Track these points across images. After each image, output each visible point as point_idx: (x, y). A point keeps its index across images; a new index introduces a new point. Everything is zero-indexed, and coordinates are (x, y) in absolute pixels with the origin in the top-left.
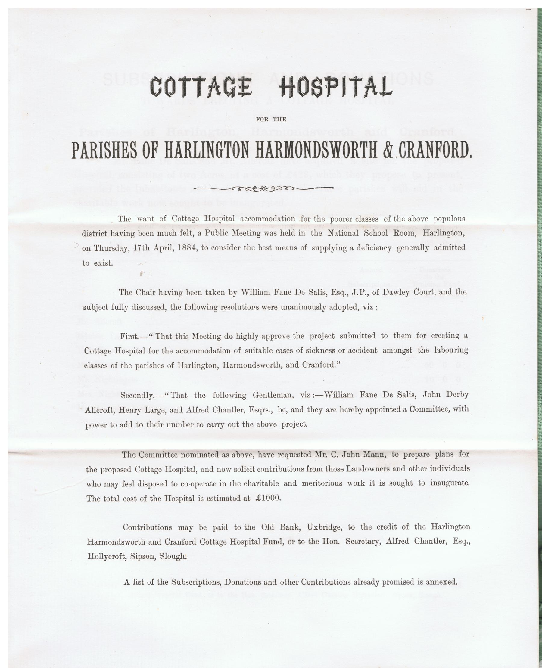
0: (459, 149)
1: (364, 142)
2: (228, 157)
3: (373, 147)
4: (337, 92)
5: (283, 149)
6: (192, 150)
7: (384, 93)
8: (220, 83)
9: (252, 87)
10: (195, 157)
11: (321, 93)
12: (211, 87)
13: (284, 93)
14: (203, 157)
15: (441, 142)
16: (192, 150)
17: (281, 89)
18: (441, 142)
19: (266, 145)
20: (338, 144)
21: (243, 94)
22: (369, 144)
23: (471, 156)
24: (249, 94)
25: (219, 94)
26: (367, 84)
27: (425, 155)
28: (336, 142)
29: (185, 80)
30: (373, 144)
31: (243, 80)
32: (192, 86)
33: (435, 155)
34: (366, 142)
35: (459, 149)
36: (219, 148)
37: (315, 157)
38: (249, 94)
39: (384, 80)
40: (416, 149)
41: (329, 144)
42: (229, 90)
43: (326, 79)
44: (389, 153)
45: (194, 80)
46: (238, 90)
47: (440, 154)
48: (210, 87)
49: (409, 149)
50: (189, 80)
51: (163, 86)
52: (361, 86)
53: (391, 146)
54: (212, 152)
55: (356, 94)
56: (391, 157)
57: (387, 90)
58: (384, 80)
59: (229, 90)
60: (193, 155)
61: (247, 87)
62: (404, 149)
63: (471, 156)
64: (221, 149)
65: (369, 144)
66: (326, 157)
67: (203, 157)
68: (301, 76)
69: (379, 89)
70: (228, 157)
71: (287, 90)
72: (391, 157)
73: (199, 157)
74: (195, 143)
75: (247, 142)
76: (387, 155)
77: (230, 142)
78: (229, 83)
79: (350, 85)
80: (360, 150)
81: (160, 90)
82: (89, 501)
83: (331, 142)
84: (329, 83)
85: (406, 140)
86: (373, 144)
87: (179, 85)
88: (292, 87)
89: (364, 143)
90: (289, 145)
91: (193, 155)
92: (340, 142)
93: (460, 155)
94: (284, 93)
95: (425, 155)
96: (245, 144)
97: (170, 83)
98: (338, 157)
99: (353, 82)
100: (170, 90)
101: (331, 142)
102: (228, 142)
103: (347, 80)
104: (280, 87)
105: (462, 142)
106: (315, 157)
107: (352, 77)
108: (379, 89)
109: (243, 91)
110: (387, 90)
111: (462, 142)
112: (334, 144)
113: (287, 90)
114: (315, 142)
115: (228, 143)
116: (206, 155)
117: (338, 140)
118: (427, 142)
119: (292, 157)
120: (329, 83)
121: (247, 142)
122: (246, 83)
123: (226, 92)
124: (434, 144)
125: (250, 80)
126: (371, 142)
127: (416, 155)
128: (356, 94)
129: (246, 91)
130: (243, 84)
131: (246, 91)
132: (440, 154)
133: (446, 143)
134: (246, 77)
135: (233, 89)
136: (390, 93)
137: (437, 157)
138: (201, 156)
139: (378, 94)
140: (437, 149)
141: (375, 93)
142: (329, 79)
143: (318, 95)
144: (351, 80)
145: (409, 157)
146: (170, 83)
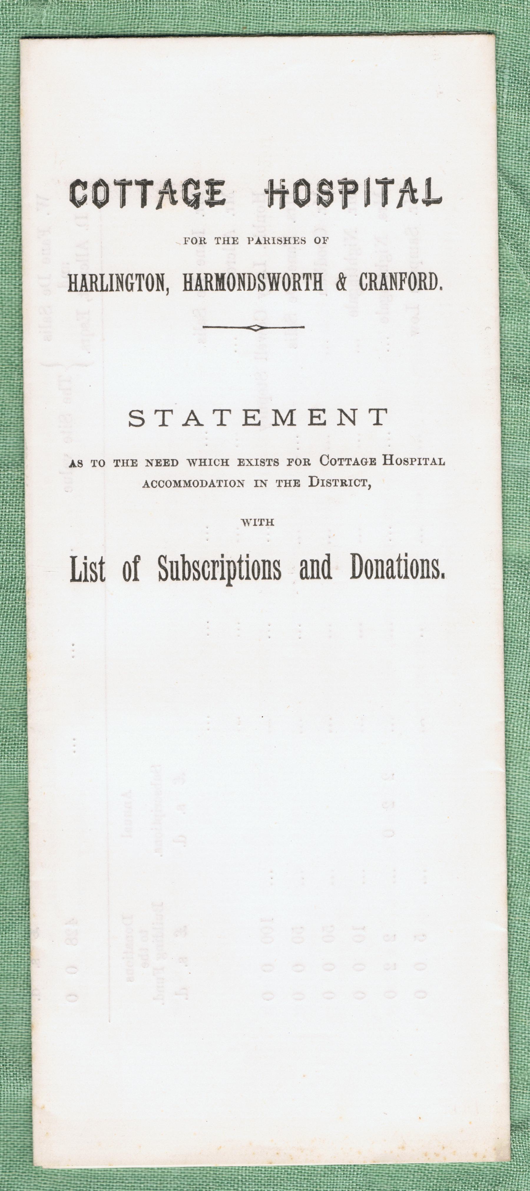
0: (428, 281)
1: (307, 274)
2: (140, 290)
3: (318, 279)
4: (357, 200)
5: (214, 282)
6: (99, 283)
7: (427, 203)
8: (177, 186)
9: (225, 192)
10: (102, 290)
11: (332, 200)
12: (162, 193)
13: (271, 203)
14: (112, 290)
15: (406, 274)
16: (99, 283)
17: (267, 196)
18: (406, 274)
19: (195, 277)
20: (276, 276)
21: (211, 204)
22: (313, 276)
23: (441, 288)
24: (222, 202)
25: (174, 202)
26: (402, 186)
27: (389, 287)
28: (274, 274)
29: (123, 184)
30: (318, 276)
31: (211, 183)
32: (134, 193)
33: (399, 287)
34: (310, 274)
35: (428, 281)
36: (130, 281)
37: (249, 289)
38: (222, 202)
39: (429, 181)
40: (379, 282)
41: (266, 276)
42: (191, 197)
43: (340, 183)
44: (343, 285)
45: (138, 183)
46: (204, 197)
47: (405, 286)
48: (160, 193)
49: (371, 280)
50: (130, 183)
51: (89, 192)
52: (394, 192)
53: (345, 278)
54: (122, 283)
55: (385, 203)
56: (344, 289)
57: (434, 196)
58: (429, 181)
59: (191, 197)
60: (99, 288)
61: (219, 192)
62: (366, 281)
63: (441, 288)
64: (132, 281)
65: (313, 276)
66: (262, 290)
67: (112, 290)
68: (296, 179)
69: (421, 195)
70: (140, 290)
71: (277, 198)
72: (344, 289)
73: (107, 290)
74: (102, 275)
75: (163, 275)
76: (340, 287)
77: (143, 275)
78: (191, 187)
79: (376, 190)
80: (303, 283)
81: (85, 198)
82: (440, 459)
83: (269, 274)
84: (346, 187)
85: (368, 271)
86: (318, 276)
87: (115, 192)
88: (283, 193)
89: (307, 276)
90: (220, 279)
91: (99, 288)
92: (279, 274)
93: (428, 287)
94: (271, 203)
95: (389, 287)
96: (161, 276)
97: (101, 190)
98: (277, 289)
99: (381, 186)
100: (101, 196)
101: (269, 274)
102: (140, 275)
103: (373, 183)
104: (267, 192)
105: (431, 274)
106: (249, 289)
107: (380, 178)
108: (421, 195)
109: (212, 198)
110: (434, 196)
111: (431, 274)
112: (271, 276)
113: (277, 198)
114: (249, 274)
115: (139, 276)
116: (115, 288)
117: (276, 271)
118: (391, 274)
119: (223, 289)
120: (346, 187)
121: (163, 275)
122: (216, 188)
123: (186, 200)
124: (398, 276)
125: (222, 183)
126: (315, 274)
127: (378, 287)
128: (385, 203)
129: (217, 198)
130: (212, 189)
131: (217, 198)
132: (405, 286)
133: (412, 275)
134: (217, 178)
135: (197, 197)
136: (439, 201)
137: (401, 289)
138: (109, 288)
139: (420, 202)
140: (401, 280)
141: (414, 201)
142: (345, 182)
143: (326, 205)
144: (378, 182)
145: (371, 289)
146: (101, 190)
